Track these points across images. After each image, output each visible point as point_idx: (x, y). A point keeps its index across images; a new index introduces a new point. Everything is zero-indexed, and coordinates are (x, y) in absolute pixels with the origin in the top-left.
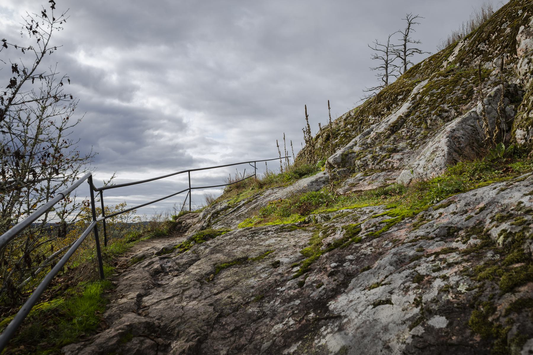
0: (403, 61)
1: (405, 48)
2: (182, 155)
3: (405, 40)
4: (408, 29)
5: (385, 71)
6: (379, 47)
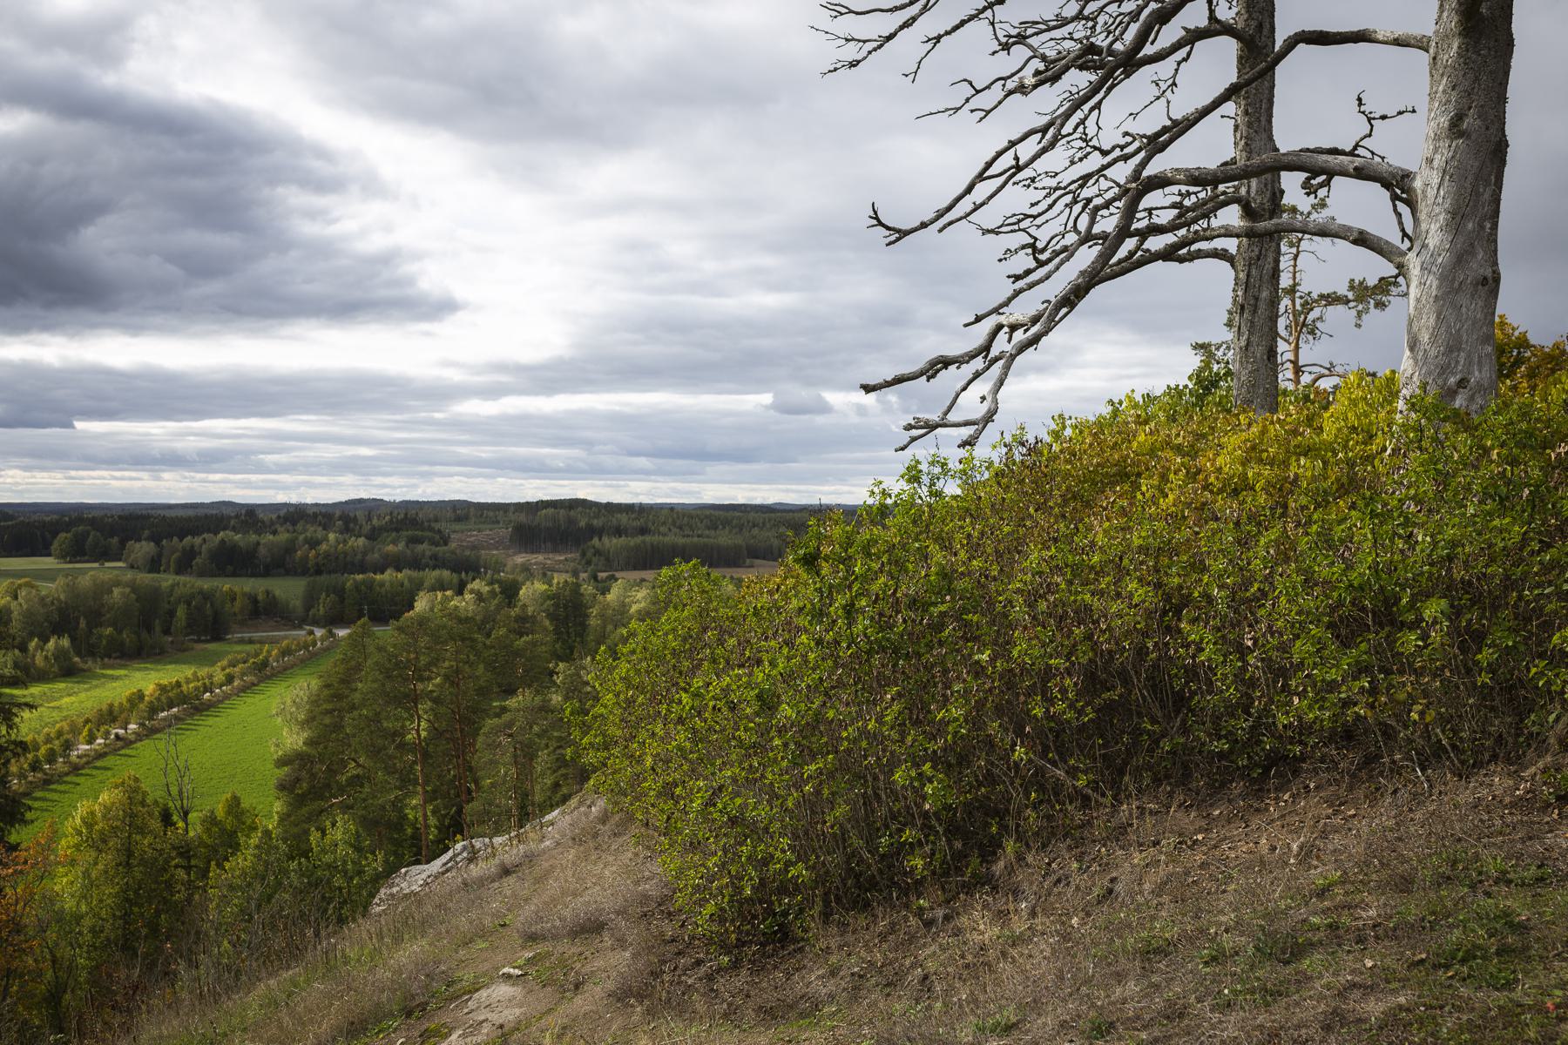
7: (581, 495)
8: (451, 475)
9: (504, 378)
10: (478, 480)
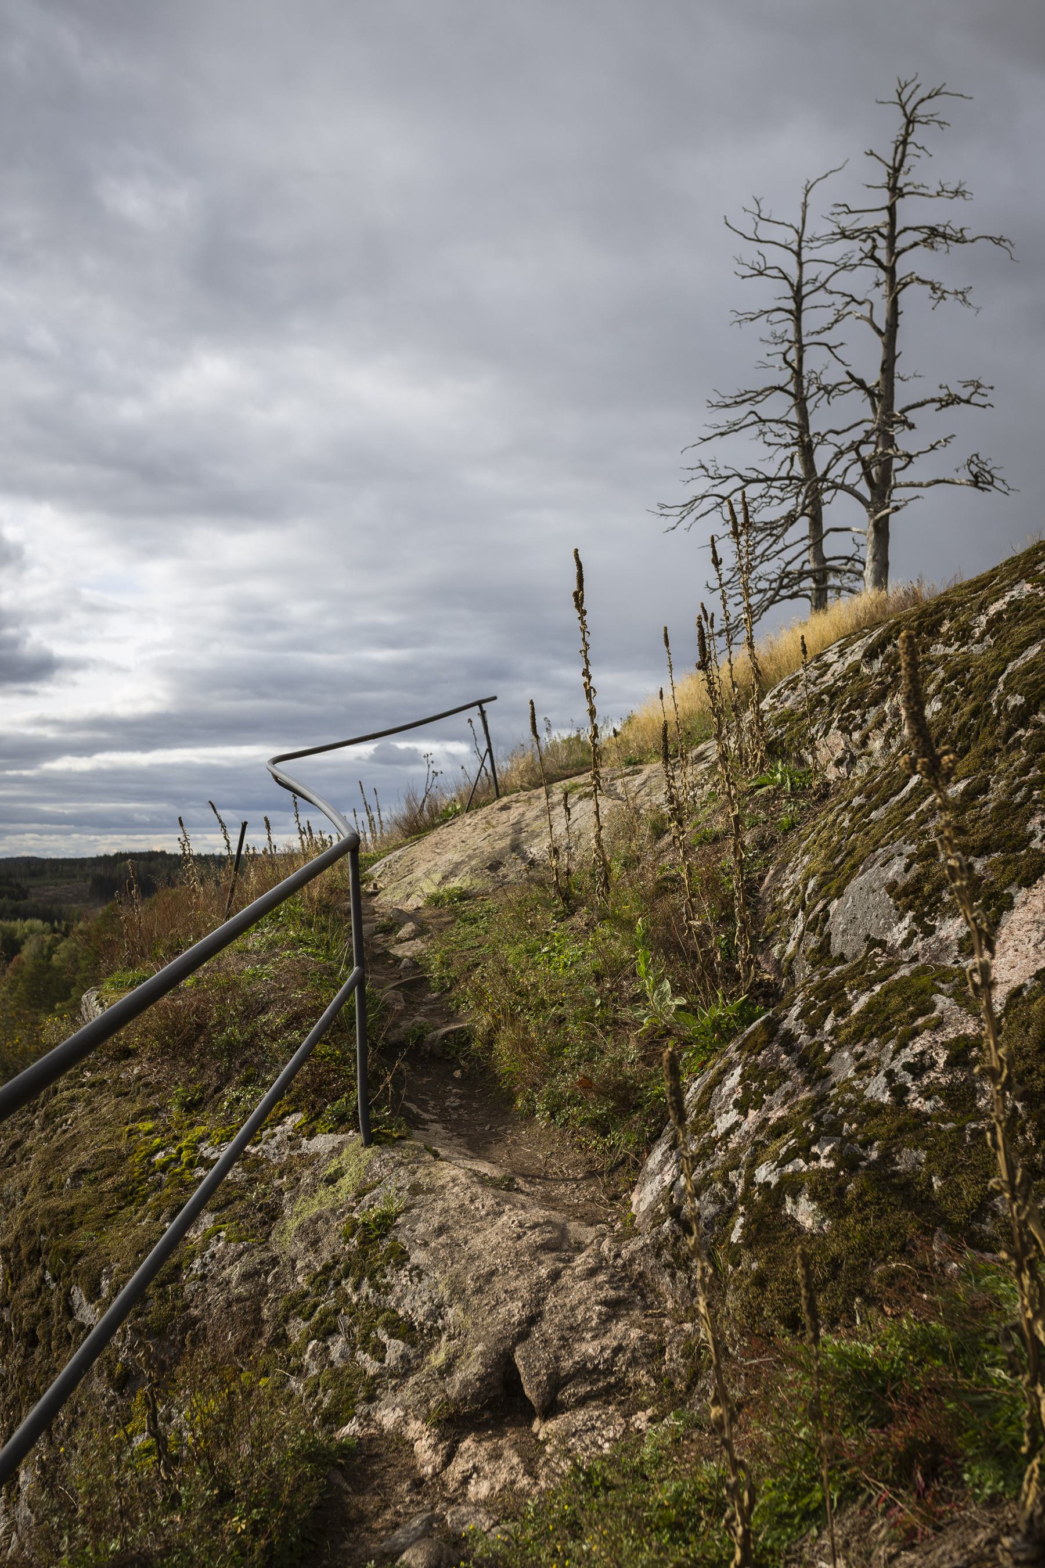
0: (883, 276)
1: (892, 223)
2: (14, 643)
3: (896, 192)
4: (904, 143)
5: (790, 326)
6: (767, 232)
7: (157, 848)
8: (23, 832)
9: (103, 735)
10: (53, 837)
